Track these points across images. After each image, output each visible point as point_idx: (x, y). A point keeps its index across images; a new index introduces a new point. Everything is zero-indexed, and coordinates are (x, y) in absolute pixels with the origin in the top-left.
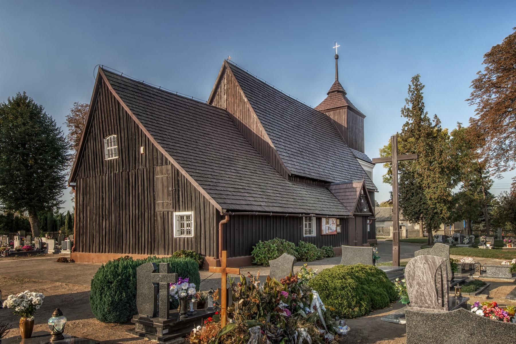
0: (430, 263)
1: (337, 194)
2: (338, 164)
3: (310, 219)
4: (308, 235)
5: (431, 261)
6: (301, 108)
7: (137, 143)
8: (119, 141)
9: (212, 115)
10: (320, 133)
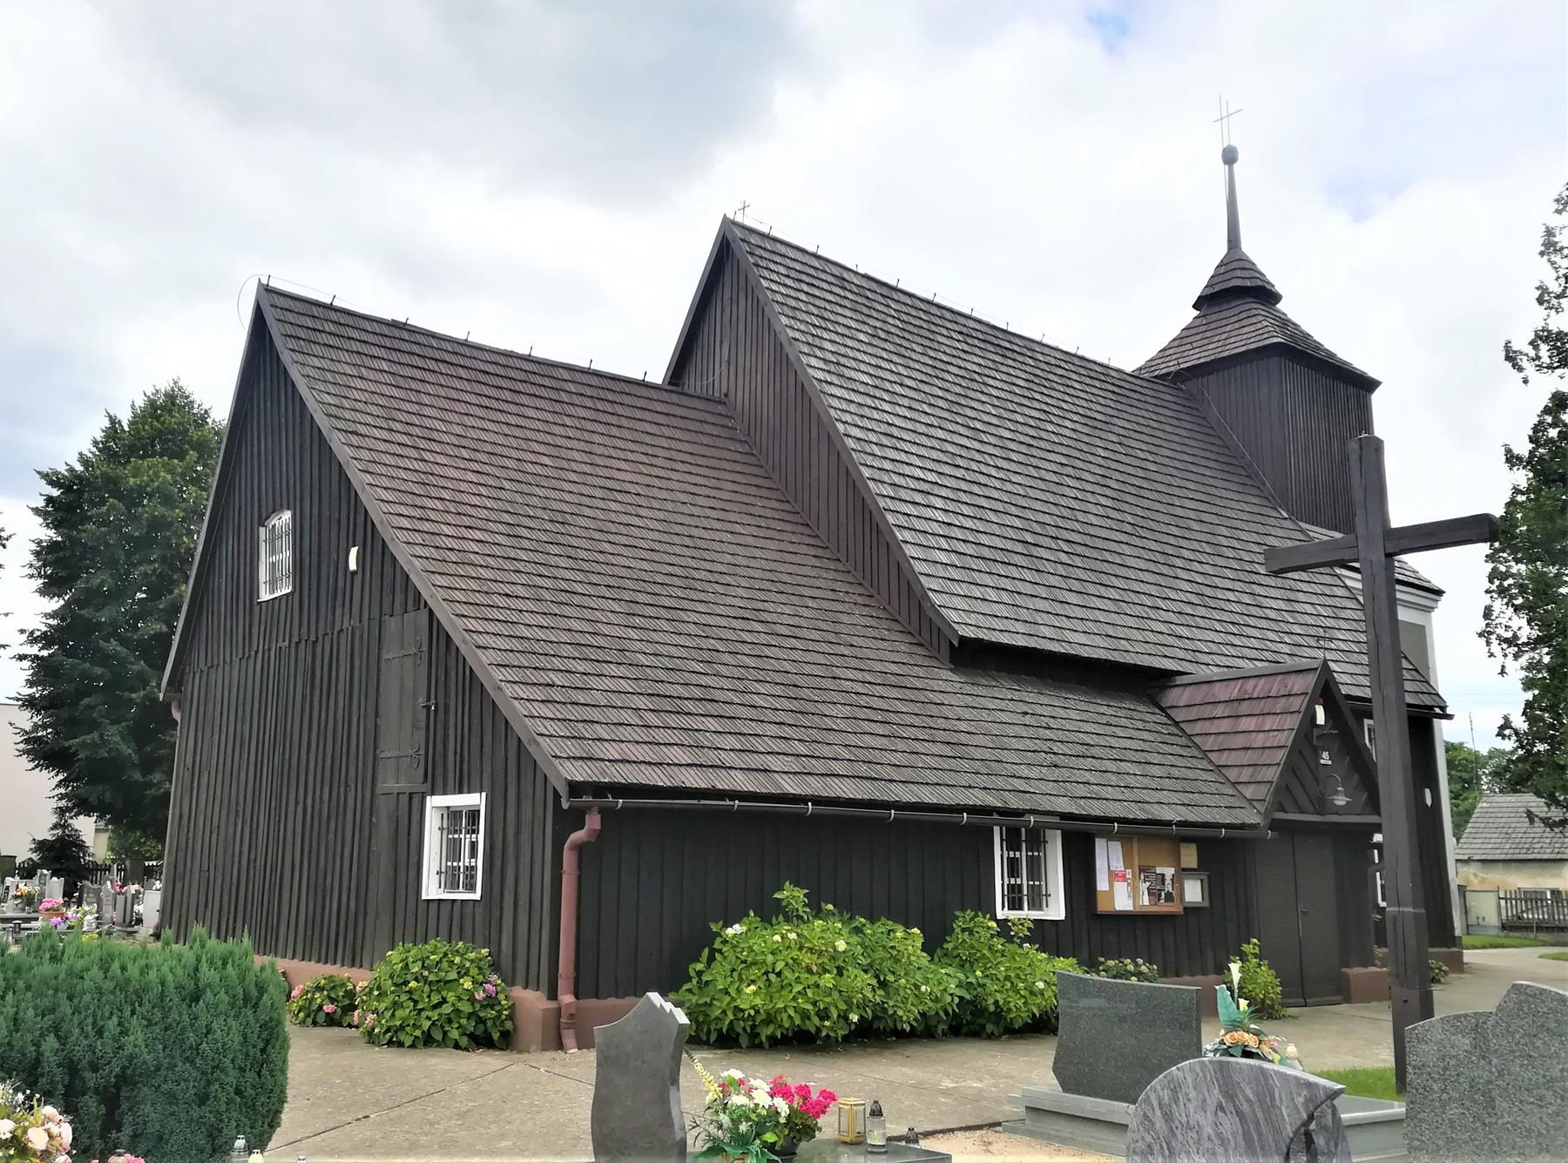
0: (1245, 1107)
1: (1198, 728)
2: (1231, 596)
3: (1036, 840)
4: (1027, 913)
5: (1249, 1092)
6: (1060, 372)
7: (342, 534)
8: (298, 530)
9: (661, 419)
10: (1144, 464)
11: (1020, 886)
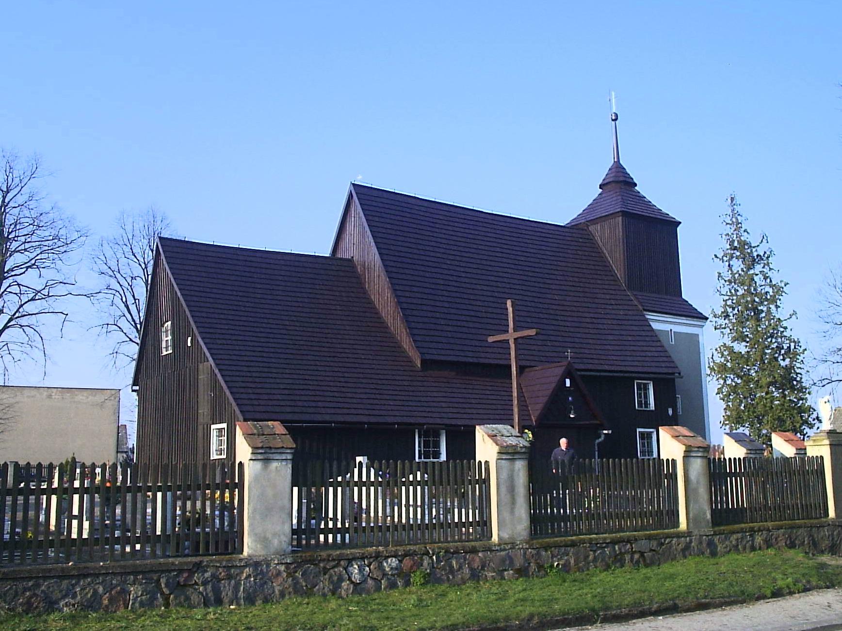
11: (424, 448)
